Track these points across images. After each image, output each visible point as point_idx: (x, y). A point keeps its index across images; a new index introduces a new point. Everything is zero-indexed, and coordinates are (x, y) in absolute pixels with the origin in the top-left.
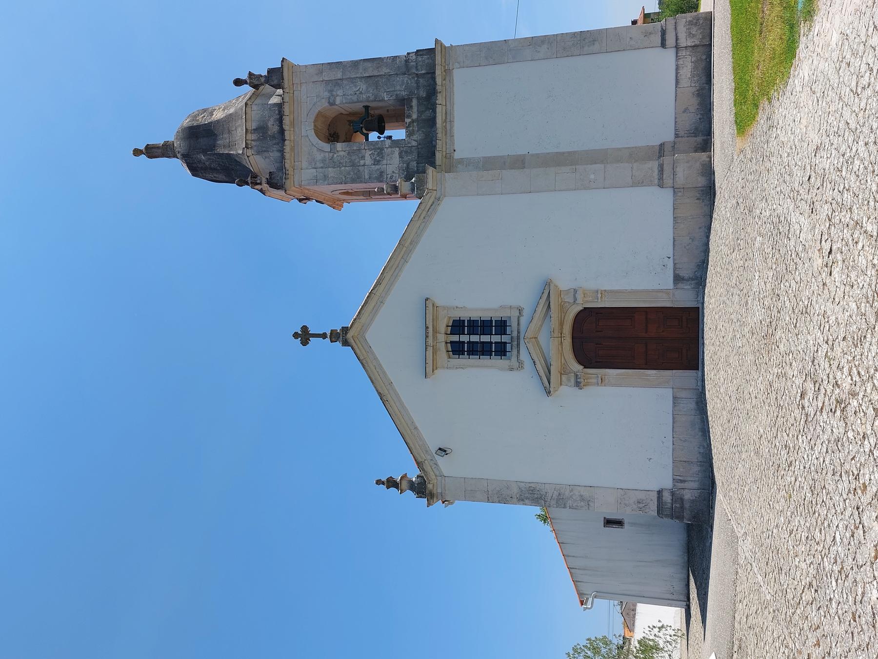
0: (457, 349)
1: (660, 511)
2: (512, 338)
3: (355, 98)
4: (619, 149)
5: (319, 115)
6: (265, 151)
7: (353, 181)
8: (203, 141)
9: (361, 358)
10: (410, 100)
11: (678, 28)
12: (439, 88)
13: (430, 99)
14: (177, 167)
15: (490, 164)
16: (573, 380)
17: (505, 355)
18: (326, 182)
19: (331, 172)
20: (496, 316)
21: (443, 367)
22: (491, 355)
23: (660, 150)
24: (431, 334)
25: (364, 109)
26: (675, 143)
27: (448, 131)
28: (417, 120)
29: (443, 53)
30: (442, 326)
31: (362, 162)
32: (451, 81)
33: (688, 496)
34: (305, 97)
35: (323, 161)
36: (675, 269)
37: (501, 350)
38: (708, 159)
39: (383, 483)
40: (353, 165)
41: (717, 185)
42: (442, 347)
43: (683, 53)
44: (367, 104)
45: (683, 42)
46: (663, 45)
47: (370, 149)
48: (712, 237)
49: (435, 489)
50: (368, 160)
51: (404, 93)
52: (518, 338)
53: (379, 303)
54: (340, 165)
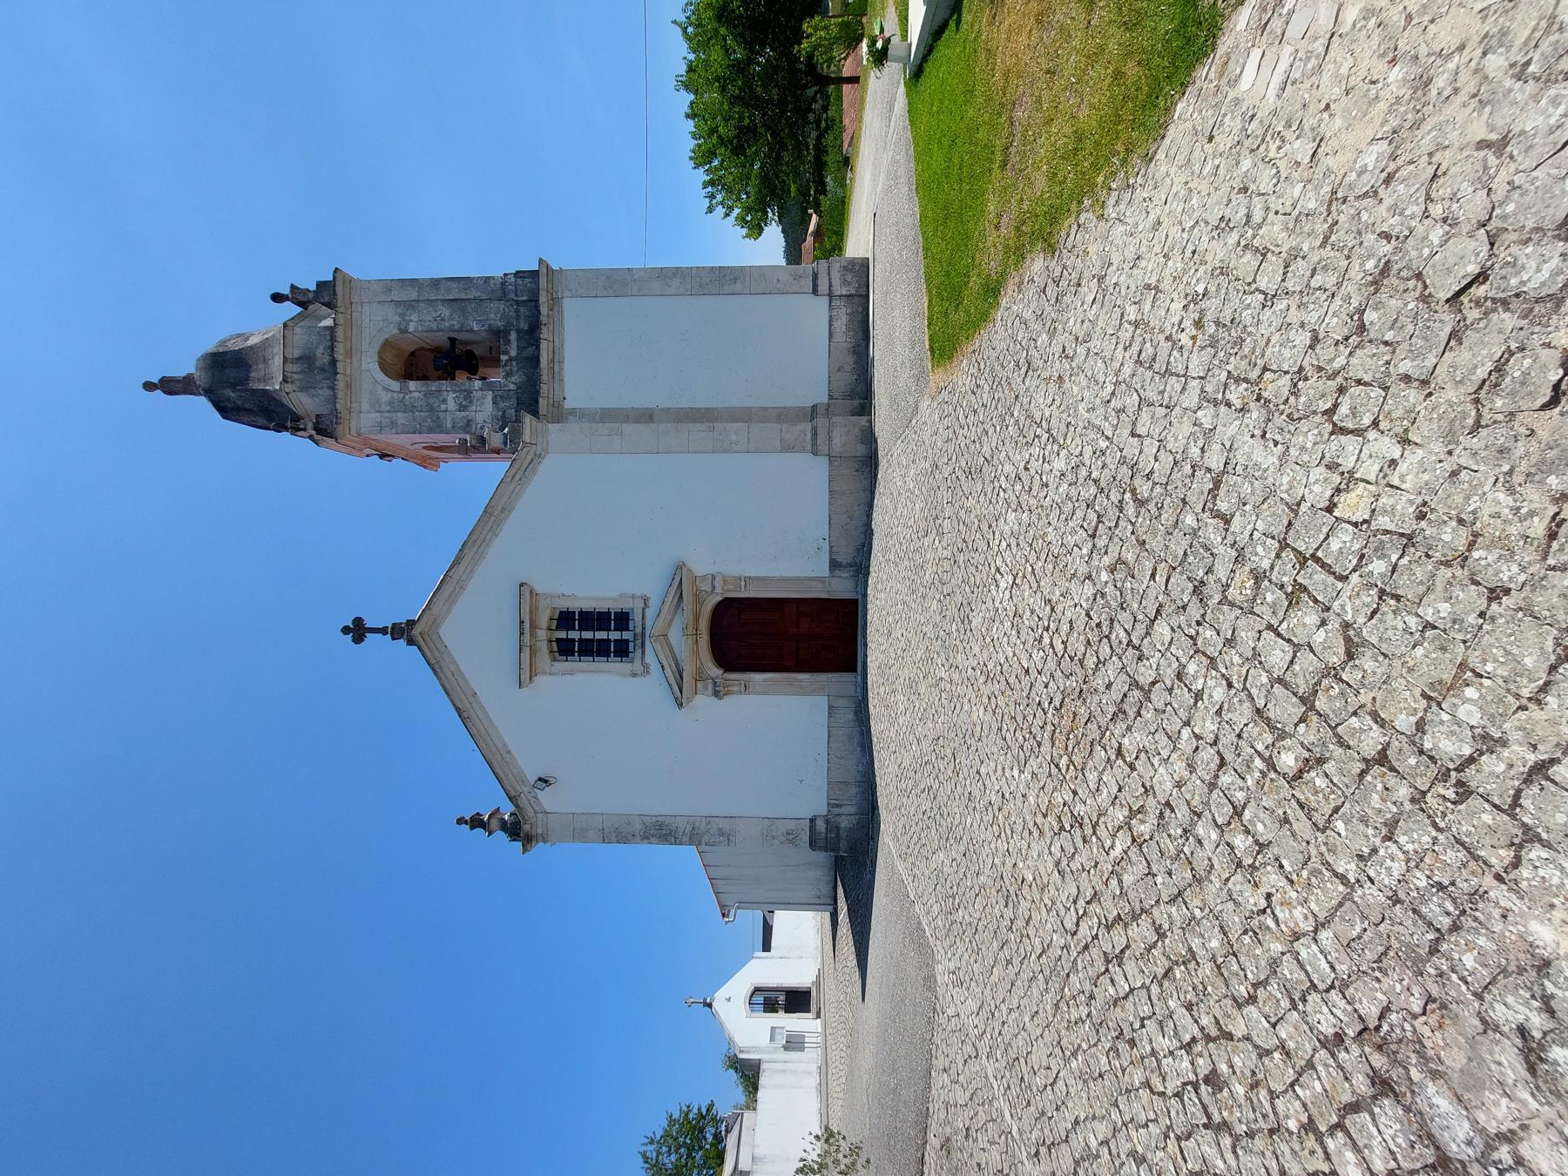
0: (565, 649)
1: (813, 844)
2: (635, 635)
3: (434, 326)
4: (766, 409)
5: (387, 345)
6: (310, 387)
7: (431, 430)
8: (231, 373)
9: (433, 661)
10: (507, 332)
11: (832, 273)
12: (543, 319)
13: (532, 334)
14: (202, 403)
15: (608, 416)
16: (710, 688)
17: (627, 656)
18: (394, 431)
19: (401, 418)
20: (615, 606)
21: (545, 673)
22: (608, 656)
23: (812, 412)
24: (527, 631)
25: (448, 344)
26: (829, 405)
27: (556, 376)
28: (516, 358)
29: (550, 277)
30: (544, 620)
31: (443, 407)
32: (561, 312)
33: (844, 823)
34: (367, 320)
35: (391, 403)
36: (831, 553)
37: (622, 650)
38: (868, 424)
39: (466, 823)
40: (431, 409)
41: (880, 453)
42: (544, 646)
43: (836, 303)
44: (454, 335)
45: (837, 291)
46: (815, 291)
47: (454, 392)
48: (877, 516)
49: (534, 829)
50: (451, 405)
51: (499, 324)
52: (643, 634)
53: (458, 589)
54: (413, 409)
